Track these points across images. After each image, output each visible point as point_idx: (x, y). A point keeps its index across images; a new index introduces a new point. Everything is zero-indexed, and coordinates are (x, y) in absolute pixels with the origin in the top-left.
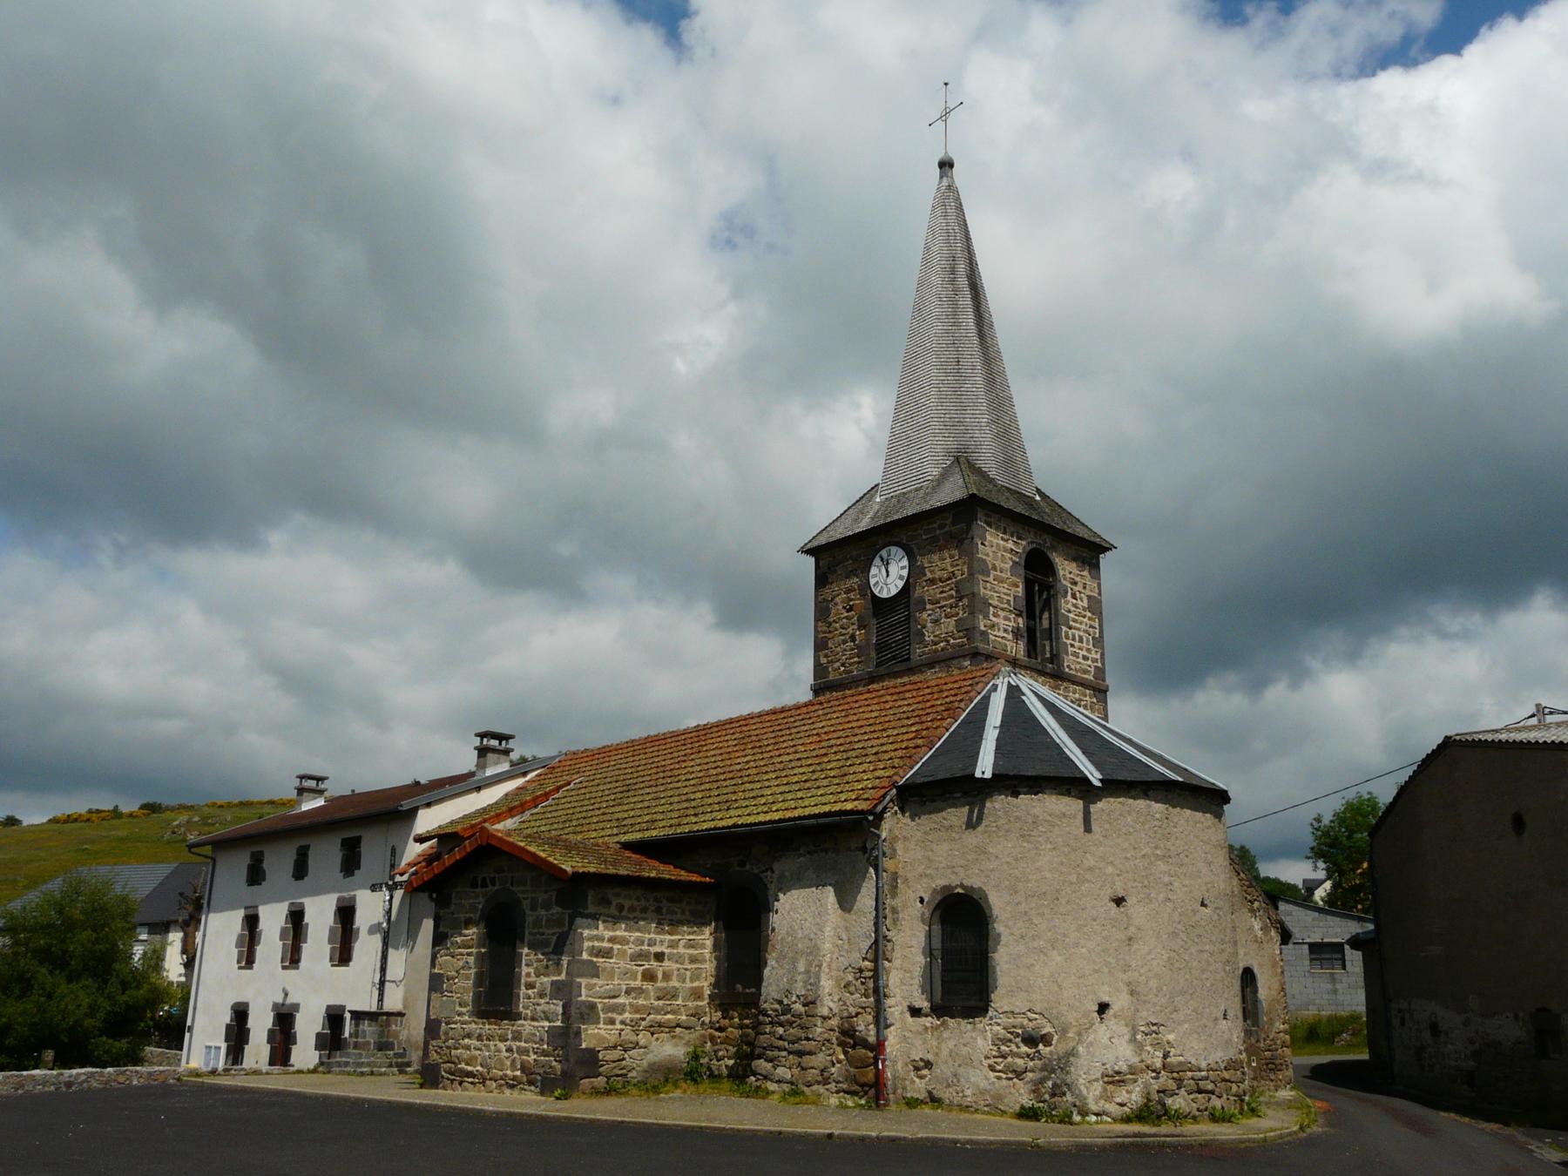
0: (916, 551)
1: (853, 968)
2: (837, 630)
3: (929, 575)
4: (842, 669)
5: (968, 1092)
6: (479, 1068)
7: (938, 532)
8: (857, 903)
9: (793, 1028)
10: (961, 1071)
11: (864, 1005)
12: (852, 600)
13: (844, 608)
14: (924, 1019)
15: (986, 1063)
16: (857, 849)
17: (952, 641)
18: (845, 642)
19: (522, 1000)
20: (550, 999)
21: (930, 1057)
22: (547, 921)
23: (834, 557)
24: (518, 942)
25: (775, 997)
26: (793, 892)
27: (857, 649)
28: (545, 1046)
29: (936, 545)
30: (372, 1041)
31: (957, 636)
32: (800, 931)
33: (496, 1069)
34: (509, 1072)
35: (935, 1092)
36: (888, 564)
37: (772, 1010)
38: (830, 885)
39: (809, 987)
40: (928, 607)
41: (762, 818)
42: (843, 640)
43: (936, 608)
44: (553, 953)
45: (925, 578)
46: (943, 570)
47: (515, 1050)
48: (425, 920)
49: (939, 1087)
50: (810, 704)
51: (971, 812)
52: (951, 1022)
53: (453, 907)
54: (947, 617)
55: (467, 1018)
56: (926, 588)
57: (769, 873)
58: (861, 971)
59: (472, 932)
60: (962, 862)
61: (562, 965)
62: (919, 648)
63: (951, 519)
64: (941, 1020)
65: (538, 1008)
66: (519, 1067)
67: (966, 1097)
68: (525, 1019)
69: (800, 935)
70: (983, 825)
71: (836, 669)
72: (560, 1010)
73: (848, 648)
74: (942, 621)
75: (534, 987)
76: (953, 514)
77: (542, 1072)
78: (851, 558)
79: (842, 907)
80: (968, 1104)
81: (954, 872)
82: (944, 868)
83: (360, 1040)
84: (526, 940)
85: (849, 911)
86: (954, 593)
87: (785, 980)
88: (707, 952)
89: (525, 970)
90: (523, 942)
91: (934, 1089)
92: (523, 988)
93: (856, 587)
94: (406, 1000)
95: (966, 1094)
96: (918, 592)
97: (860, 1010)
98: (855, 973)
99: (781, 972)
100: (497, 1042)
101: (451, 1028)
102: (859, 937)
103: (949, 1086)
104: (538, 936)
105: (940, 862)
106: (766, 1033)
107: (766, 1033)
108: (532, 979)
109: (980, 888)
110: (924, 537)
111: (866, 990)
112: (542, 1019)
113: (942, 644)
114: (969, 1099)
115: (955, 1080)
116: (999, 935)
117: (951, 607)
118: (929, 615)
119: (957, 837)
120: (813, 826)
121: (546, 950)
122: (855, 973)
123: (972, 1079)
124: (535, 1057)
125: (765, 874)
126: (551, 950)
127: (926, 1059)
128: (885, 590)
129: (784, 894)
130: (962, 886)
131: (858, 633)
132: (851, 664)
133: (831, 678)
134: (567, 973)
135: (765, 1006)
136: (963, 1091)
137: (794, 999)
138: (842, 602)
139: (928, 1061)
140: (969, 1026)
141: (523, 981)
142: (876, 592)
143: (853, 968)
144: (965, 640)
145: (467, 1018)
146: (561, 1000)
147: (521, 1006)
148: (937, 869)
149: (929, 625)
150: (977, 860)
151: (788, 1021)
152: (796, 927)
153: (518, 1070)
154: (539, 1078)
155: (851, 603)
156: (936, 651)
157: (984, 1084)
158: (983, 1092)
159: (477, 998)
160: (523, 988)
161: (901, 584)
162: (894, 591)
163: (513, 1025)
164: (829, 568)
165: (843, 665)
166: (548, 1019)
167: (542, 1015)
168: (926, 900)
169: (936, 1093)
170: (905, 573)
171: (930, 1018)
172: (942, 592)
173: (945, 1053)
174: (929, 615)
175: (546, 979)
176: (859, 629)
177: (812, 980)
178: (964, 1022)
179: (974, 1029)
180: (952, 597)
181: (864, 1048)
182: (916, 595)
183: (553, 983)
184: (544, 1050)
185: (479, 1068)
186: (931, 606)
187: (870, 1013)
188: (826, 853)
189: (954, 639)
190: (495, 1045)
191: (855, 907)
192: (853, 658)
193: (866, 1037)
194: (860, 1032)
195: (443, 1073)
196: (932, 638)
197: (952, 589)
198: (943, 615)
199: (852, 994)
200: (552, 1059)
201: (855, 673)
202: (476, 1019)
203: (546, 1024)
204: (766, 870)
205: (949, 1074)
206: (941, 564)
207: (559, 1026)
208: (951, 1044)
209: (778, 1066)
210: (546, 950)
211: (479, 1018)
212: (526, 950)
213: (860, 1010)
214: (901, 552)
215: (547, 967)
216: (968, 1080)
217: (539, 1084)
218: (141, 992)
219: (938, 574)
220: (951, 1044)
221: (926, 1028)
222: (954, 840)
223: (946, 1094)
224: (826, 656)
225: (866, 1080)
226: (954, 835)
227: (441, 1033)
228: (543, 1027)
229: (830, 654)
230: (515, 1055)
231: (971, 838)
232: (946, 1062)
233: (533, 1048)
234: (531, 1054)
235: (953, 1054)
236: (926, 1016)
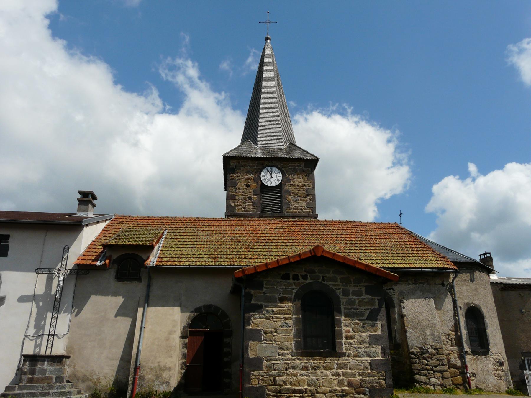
0: (285, 172)
1: (445, 334)
2: (240, 193)
3: (292, 183)
4: (243, 209)
5: (490, 385)
6: (306, 387)
7: (296, 168)
8: (444, 307)
9: (432, 360)
10: (486, 377)
11: (453, 350)
12: (250, 183)
13: (245, 184)
14: (469, 356)
15: (493, 373)
16: (439, 284)
17: (304, 210)
18: (245, 199)
19: (344, 346)
20: (369, 344)
21: (475, 371)
22: (359, 302)
23: (239, 163)
24: (335, 313)
25: (418, 346)
26: (412, 300)
27: (252, 203)
28: (369, 371)
29: (295, 172)
30: (54, 376)
31: (307, 208)
32: (421, 317)
33: (324, 387)
34: (337, 388)
35: (479, 386)
36: (271, 173)
37: (417, 352)
38: (432, 298)
39: (436, 342)
40: (292, 194)
41: (401, 266)
42: (244, 198)
43: (296, 196)
44: (367, 319)
45: (290, 183)
46: (300, 182)
47: (341, 374)
48: (121, 297)
49: (480, 384)
50: (222, 219)
51: (471, 276)
52: (479, 357)
53: (264, 290)
54: (301, 200)
55: (290, 356)
56: (290, 187)
57: (391, 290)
58: (449, 335)
59: (287, 305)
60: (471, 294)
61: (377, 327)
62: (287, 209)
63: (303, 165)
64: (475, 356)
65: (360, 350)
66: (346, 384)
67: (490, 387)
68: (348, 356)
69: (422, 319)
70: (475, 281)
71: (240, 209)
72: (380, 351)
73: (247, 201)
74: (299, 201)
75: (354, 338)
76: (304, 163)
77: (369, 386)
78: (249, 166)
79: (437, 309)
80: (491, 390)
81: (469, 298)
82: (466, 296)
83: (36, 376)
84: (343, 312)
85: (440, 310)
86: (305, 192)
87: (421, 338)
88: (290, 322)
89: (344, 329)
90: (340, 312)
91: (478, 385)
92: (344, 339)
93: (252, 178)
94: (69, 348)
95: (490, 386)
96: (286, 188)
97: (451, 352)
98: (445, 336)
99: (417, 335)
100: (323, 371)
101: (274, 364)
102: (446, 321)
103: (483, 383)
104: (353, 310)
105: (464, 293)
106: (416, 363)
107: (416, 363)
108: (352, 333)
109: (478, 305)
110: (289, 168)
111: (452, 343)
112: (364, 356)
113: (299, 210)
114: (491, 388)
115: (485, 381)
116: (487, 323)
117: (303, 197)
118: (292, 198)
119: (468, 285)
120: (431, 272)
121: (361, 318)
122: (445, 336)
123: (490, 380)
124: (361, 377)
125: (390, 291)
126: (365, 318)
127: (473, 373)
128: (269, 182)
129: (406, 300)
130: (472, 303)
131: (253, 196)
132: (249, 208)
133: (236, 212)
134: (382, 330)
135: (412, 350)
136: (488, 385)
137: (429, 347)
138: (244, 182)
139: (474, 373)
140: (485, 359)
141: (344, 335)
142: (265, 183)
143: (445, 334)
144: (311, 211)
145: (290, 356)
146: (379, 345)
147: (344, 349)
148: (464, 296)
149: (292, 201)
150: (476, 294)
151: (428, 357)
152: (419, 315)
153: (345, 386)
154: (367, 390)
155: (249, 184)
156: (296, 213)
157: (494, 382)
158: (495, 385)
159: (297, 345)
160: (344, 339)
161: (278, 183)
162: (274, 185)
163: (338, 360)
164: (236, 167)
165: (244, 208)
166: (370, 356)
167: (364, 354)
168: (462, 308)
169: (480, 387)
170: (280, 179)
171: (471, 356)
172: (299, 191)
173: (480, 370)
174: (292, 198)
175: (364, 334)
176: (254, 195)
177: (437, 339)
178: (483, 357)
179: (487, 360)
180: (304, 194)
181: (454, 368)
182: (285, 189)
183: (370, 336)
184: (369, 373)
185: (306, 387)
186: (293, 195)
187: (456, 353)
188: (424, 284)
189: (305, 209)
190: (322, 373)
191: (442, 308)
192: (250, 206)
193: (456, 364)
194: (452, 361)
195: (268, 392)
196: (293, 206)
197: (304, 191)
198: (299, 199)
199: (445, 345)
200: (377, 378)
201: (251, 212)
202: (300, 357)
203: (368, 359)
204: (390, 289)
205: (483, 378)
206: (298, 180)
207: (380, 360)
208: (481, 366)
209: (430, 378)
210: (361, 318)
211: (302, 356)
212: (343, 318)
213: (451, 352)
214: (278, 171)
215: (363, 327)
216: (489, 380)
217: (368, 393)
218: (397, 324)
219: (297, 184)
220: (481, 366)
221: (471, 360)
222: (467, 285)
223: (483, 387)
224: (234, 202)
225: (458, 382)
226: (467, 283)
227: (263, 367)
228: (366, 360)
229: (236, 202)
230: (342, 377)
231: (472, 285)
232: (481, 374)
233: (359, 373)
234: (357, 376)
235: (483, 370)
236: (469, 355)
